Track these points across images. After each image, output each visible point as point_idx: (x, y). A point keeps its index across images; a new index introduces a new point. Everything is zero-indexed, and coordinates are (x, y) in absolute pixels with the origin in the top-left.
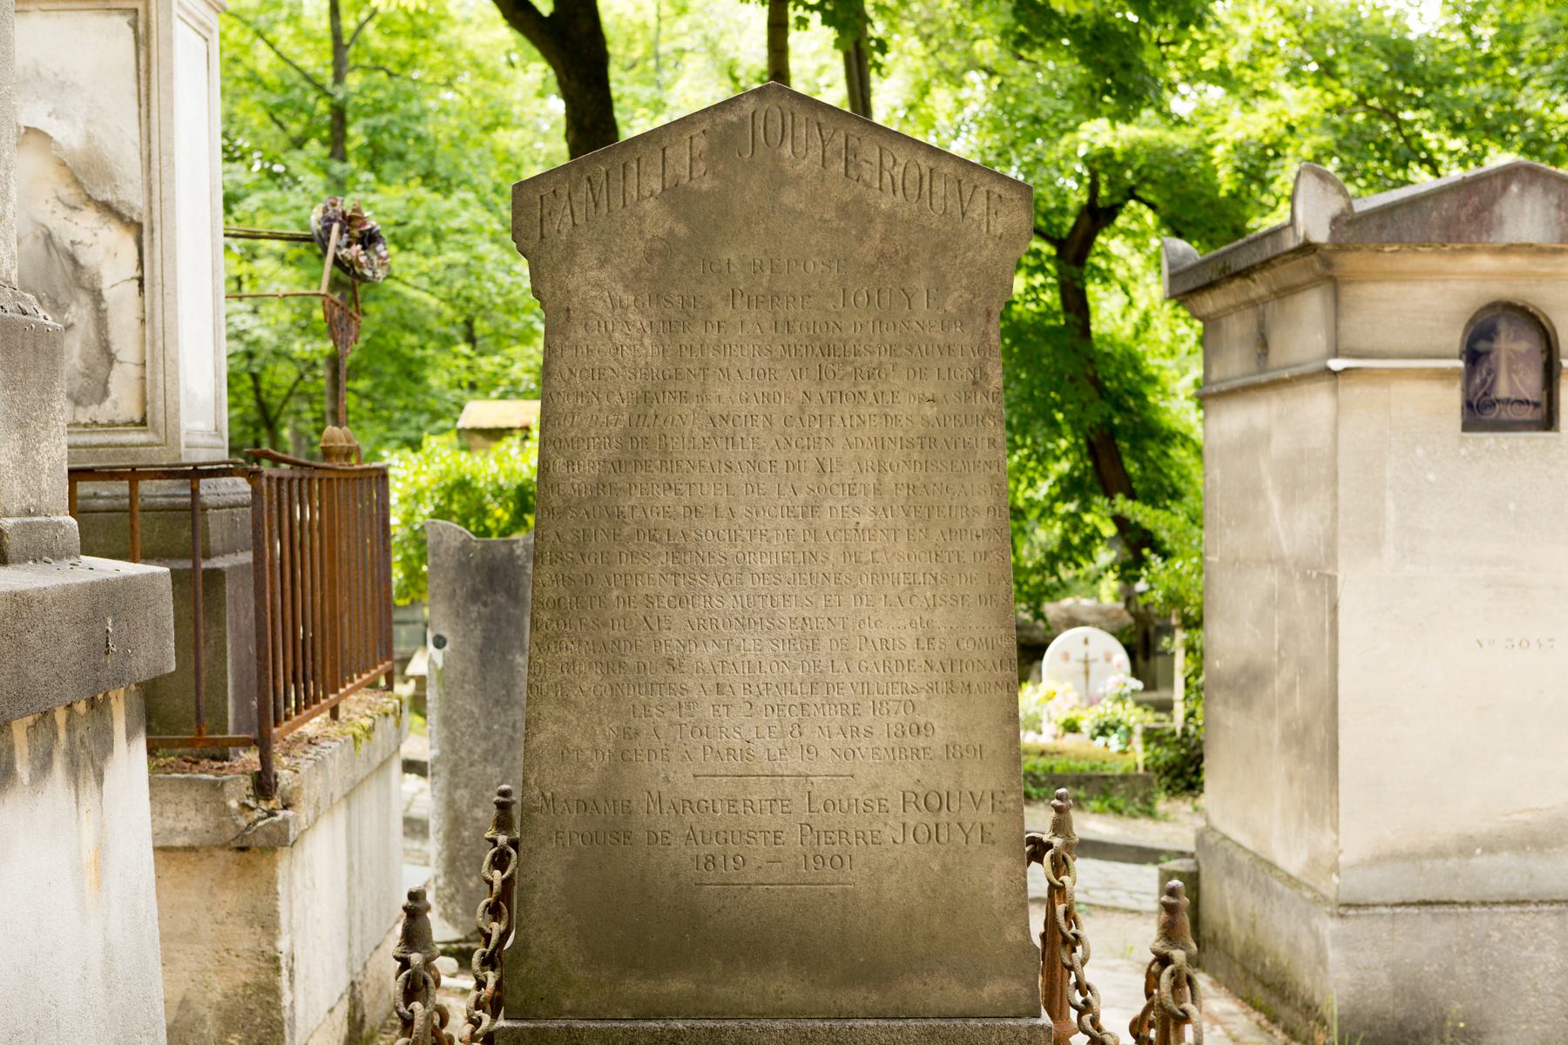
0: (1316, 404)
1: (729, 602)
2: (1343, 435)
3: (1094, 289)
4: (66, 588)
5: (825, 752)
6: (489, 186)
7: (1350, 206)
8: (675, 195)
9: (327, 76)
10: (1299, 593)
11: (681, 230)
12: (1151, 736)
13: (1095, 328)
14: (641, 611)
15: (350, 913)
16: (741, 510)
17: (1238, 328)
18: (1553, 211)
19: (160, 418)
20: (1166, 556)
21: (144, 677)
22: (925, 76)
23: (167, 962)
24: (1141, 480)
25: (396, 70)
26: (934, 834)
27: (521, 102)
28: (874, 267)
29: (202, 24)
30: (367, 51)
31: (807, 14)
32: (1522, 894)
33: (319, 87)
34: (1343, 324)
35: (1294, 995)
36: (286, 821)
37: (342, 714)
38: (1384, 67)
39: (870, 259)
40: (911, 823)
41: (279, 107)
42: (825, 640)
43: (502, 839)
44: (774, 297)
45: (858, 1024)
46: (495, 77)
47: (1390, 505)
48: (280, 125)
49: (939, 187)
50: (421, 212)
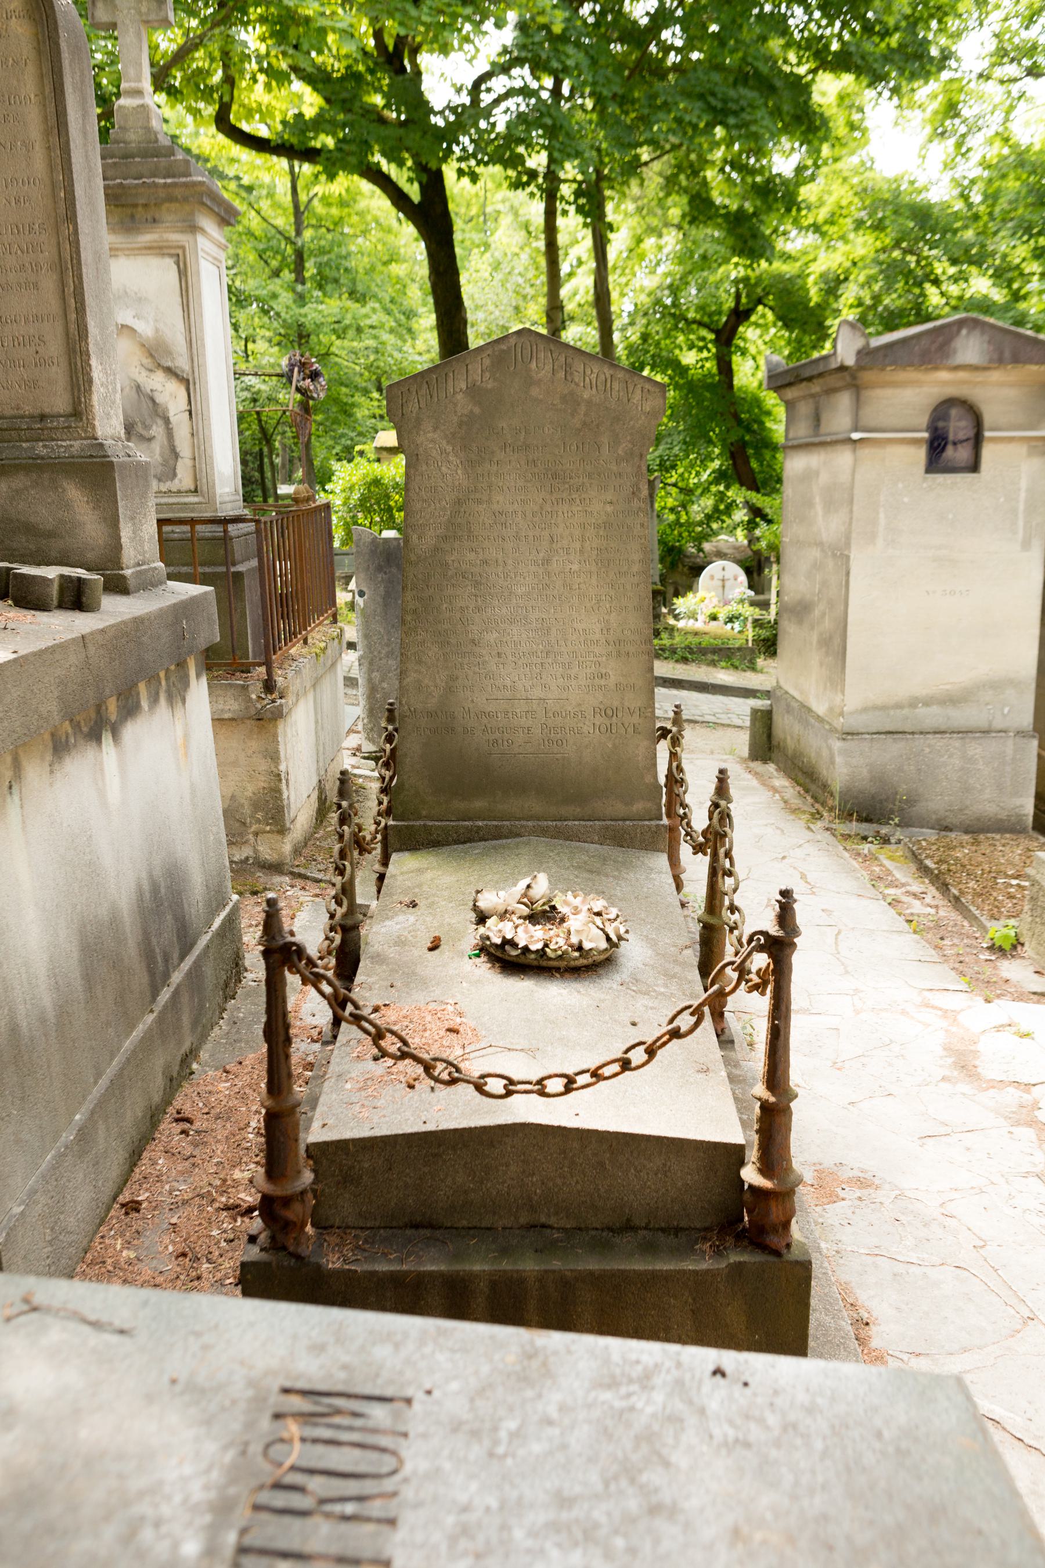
0: (844, 458)
1: (504, 610)
2: (858, 477)
3: (736, 359)
4: (161, 609)
5: (554, 688)
6: (388, 299)
7: (868, 344)
8: (474, 392)
9: (293, 234)
10: (830, 564)
11: (477, 410)
12: (757, 623)
13: (736, 382)
14: (458, 615)
15: (317, 744)
16: (510, 562)
17: (804, 409)
18: (985, 345)
19: (205, 488)
20: (769, 522)
21: (204, 647)
22: (639, 231)
23: (222, 776)
24: (760, 472)
25: (331, 227)
26: (609, 729)
27: (405, 246)
28: (580, 430)
29: (215, 259)
30: (314, 214)
31: (567, 207)
32: (943, 728)
33: (288, 239)
34: (861, 413)
35: (818, 779)
36: (281, 705)
37: (310, 641)
38: (911, 224)
39: (578, 426)
40: (598, 723)
41: (264, 251)
42: (554, 630)
43: (390, 728)
44: (527, 447)
45: (570, 823)
46: (389, 231)
47: (882, 516)
48: (266, 262)
49: (616, 386)
50: (349, 316)
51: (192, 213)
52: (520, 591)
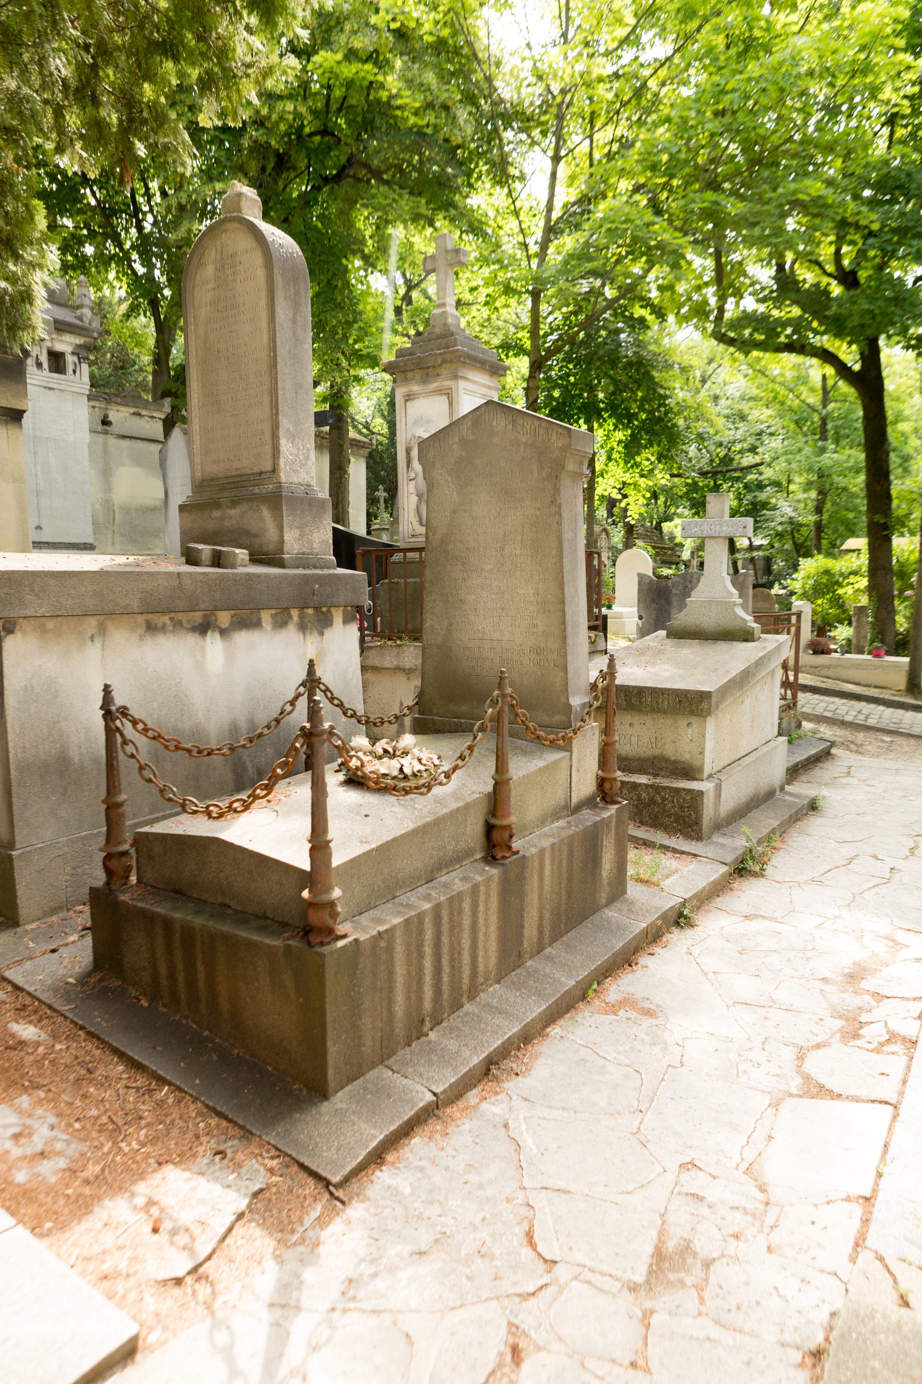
8: (463, 443)
11: (464, 454)
49: (541, 432)
51: (457, 369)
52: (487, 567)
